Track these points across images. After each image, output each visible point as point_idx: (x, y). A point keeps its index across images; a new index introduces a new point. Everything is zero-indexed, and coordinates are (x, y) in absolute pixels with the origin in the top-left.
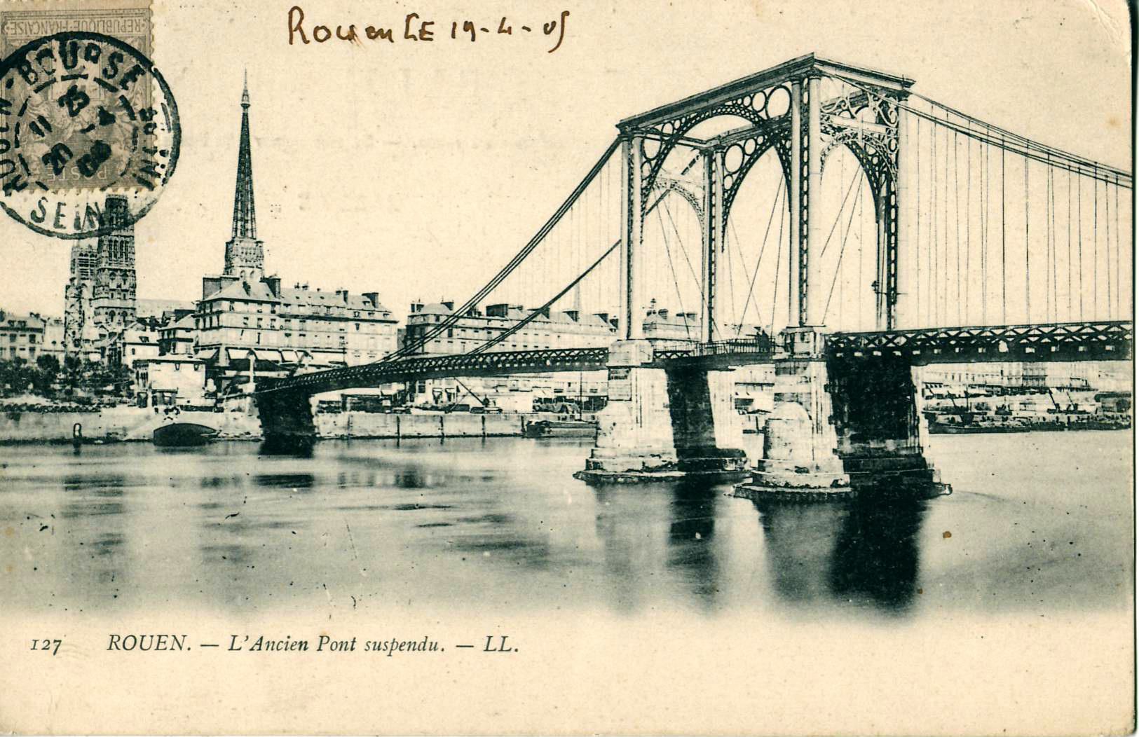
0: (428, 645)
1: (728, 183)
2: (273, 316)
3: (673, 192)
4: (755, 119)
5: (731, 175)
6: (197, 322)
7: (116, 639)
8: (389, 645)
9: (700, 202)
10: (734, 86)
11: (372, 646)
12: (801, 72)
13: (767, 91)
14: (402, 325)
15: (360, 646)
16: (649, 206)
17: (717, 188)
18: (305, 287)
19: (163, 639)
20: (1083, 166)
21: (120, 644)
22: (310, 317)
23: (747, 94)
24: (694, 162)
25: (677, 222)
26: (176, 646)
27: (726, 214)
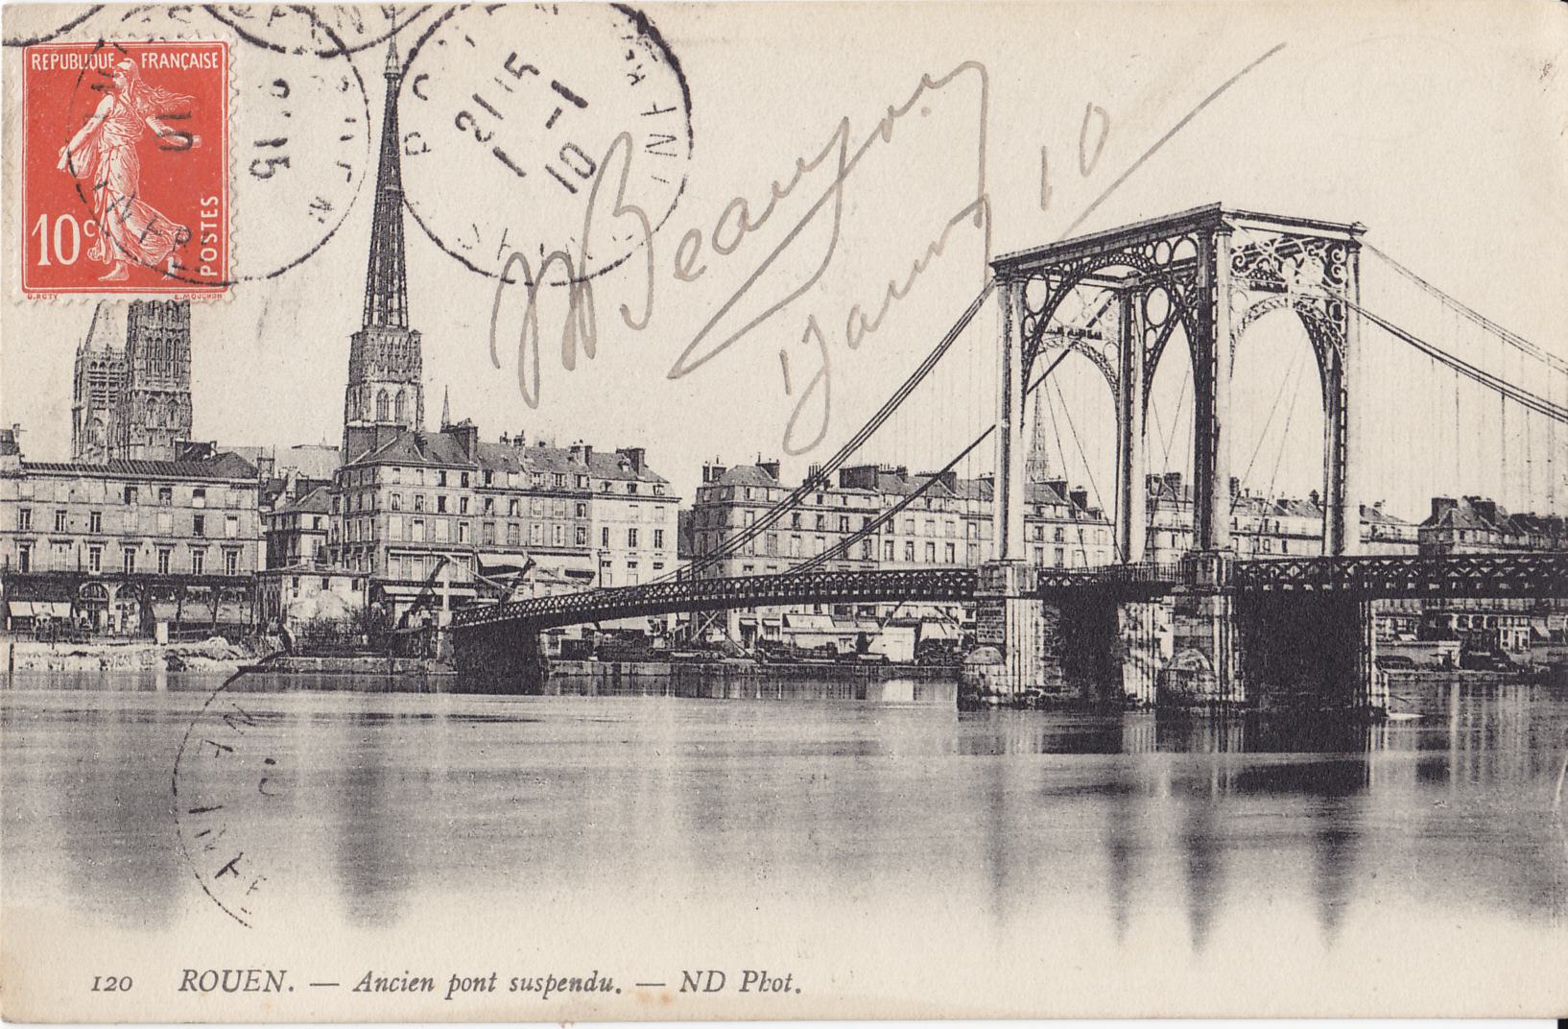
0: (597, 984)
1: (1152, 339)
2: (464, 492)
3: (1073, 351)
4: (1165, 276)
5: (1154, 328)
6: (336, 501)
7: (191, 975)
8: (544, 984)
9: (1115, 365)
10: (1136, 231)
11: (487, 984)
12: (1208, 223)
13: (1172, 241)
14: (687, 504)
15: (442, 986)
16: (1032, 382)
17: (1137, 348)
18: (519, 441)
19: (254, 976)
20: (1529, 403)
21: (196, 983)
22: (525, 493)
23: (1149, 242)
24: (1104, 309)
25: (1079, 390)
26: (272, 986)
27: (1146, 392)
